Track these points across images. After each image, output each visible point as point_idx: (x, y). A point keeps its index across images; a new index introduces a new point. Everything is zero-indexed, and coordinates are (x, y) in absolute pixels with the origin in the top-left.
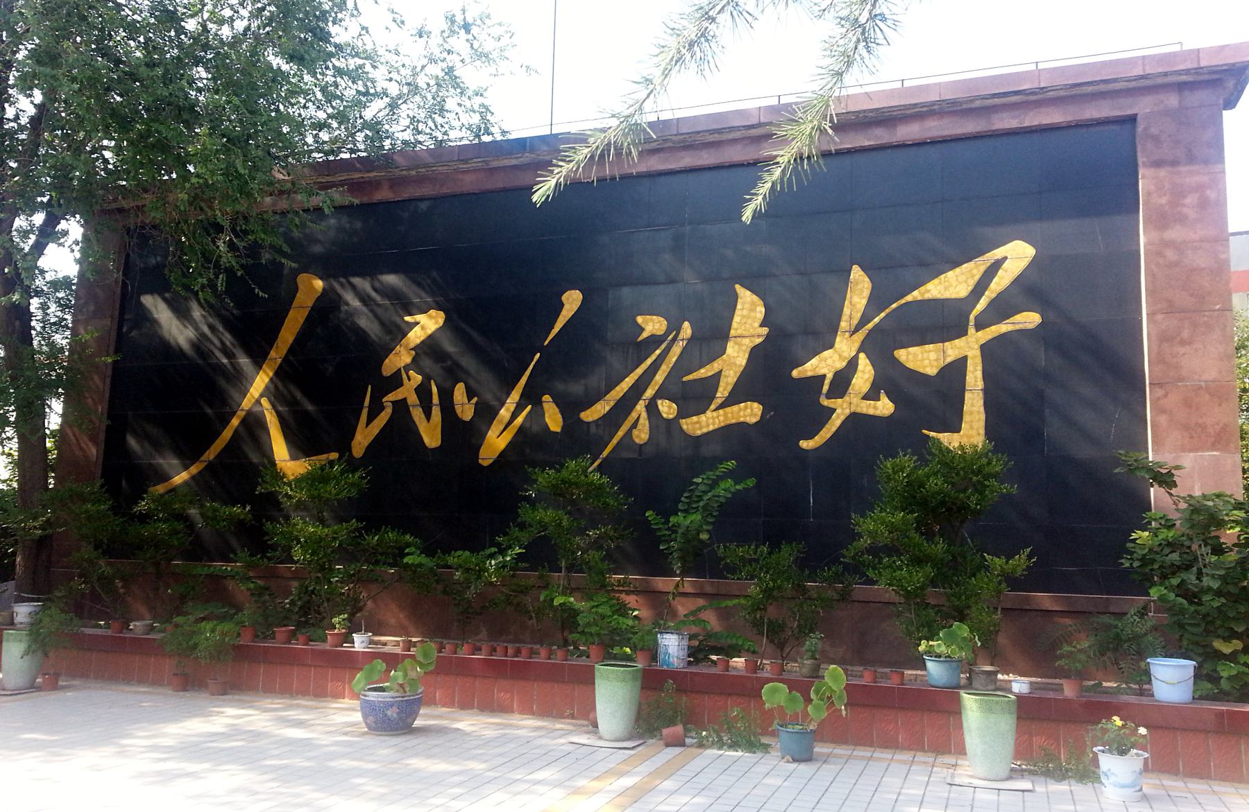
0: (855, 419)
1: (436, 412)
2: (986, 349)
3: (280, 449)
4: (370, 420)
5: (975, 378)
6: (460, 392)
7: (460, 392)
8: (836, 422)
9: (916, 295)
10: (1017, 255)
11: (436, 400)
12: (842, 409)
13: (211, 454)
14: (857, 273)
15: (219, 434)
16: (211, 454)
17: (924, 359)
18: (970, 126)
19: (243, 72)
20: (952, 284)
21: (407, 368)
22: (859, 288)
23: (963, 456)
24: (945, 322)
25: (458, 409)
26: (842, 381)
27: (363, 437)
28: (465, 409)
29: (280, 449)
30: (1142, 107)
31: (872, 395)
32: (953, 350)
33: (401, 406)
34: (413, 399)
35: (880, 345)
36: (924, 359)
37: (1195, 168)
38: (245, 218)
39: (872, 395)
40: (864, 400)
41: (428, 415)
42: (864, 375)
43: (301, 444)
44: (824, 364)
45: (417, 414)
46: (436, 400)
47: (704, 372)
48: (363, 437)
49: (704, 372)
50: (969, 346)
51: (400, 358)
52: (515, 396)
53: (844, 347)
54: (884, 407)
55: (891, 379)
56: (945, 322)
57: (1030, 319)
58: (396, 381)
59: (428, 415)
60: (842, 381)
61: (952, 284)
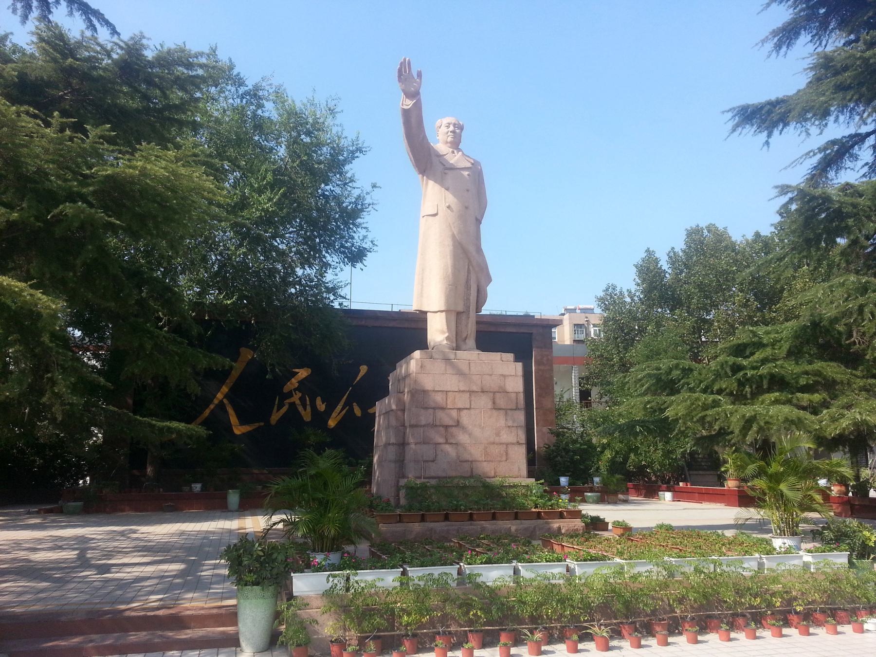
1: (309, 408)
3: (233, 419)
4: (278, 410)
6: (319, 401)
7: (319, 401)
11: (308, 403)
15: (201, 413)
18: (493, 329)
21: (295, 390)
23: (626, 492)
25: (318, 407)
27: (275, 417)
28: (321, 406)
29: (233, 419)
33: (293, 405)
34: (298, 402)
38: (786, 592)
41: (305, 409)
43: (243, 420)
45: (300, 409)
46: (308, 403)
47: (297, 370)
48: (275, 417)
49: (297, 370)
52: (203, 574)
58: (290, 394)
59: (305, 409)
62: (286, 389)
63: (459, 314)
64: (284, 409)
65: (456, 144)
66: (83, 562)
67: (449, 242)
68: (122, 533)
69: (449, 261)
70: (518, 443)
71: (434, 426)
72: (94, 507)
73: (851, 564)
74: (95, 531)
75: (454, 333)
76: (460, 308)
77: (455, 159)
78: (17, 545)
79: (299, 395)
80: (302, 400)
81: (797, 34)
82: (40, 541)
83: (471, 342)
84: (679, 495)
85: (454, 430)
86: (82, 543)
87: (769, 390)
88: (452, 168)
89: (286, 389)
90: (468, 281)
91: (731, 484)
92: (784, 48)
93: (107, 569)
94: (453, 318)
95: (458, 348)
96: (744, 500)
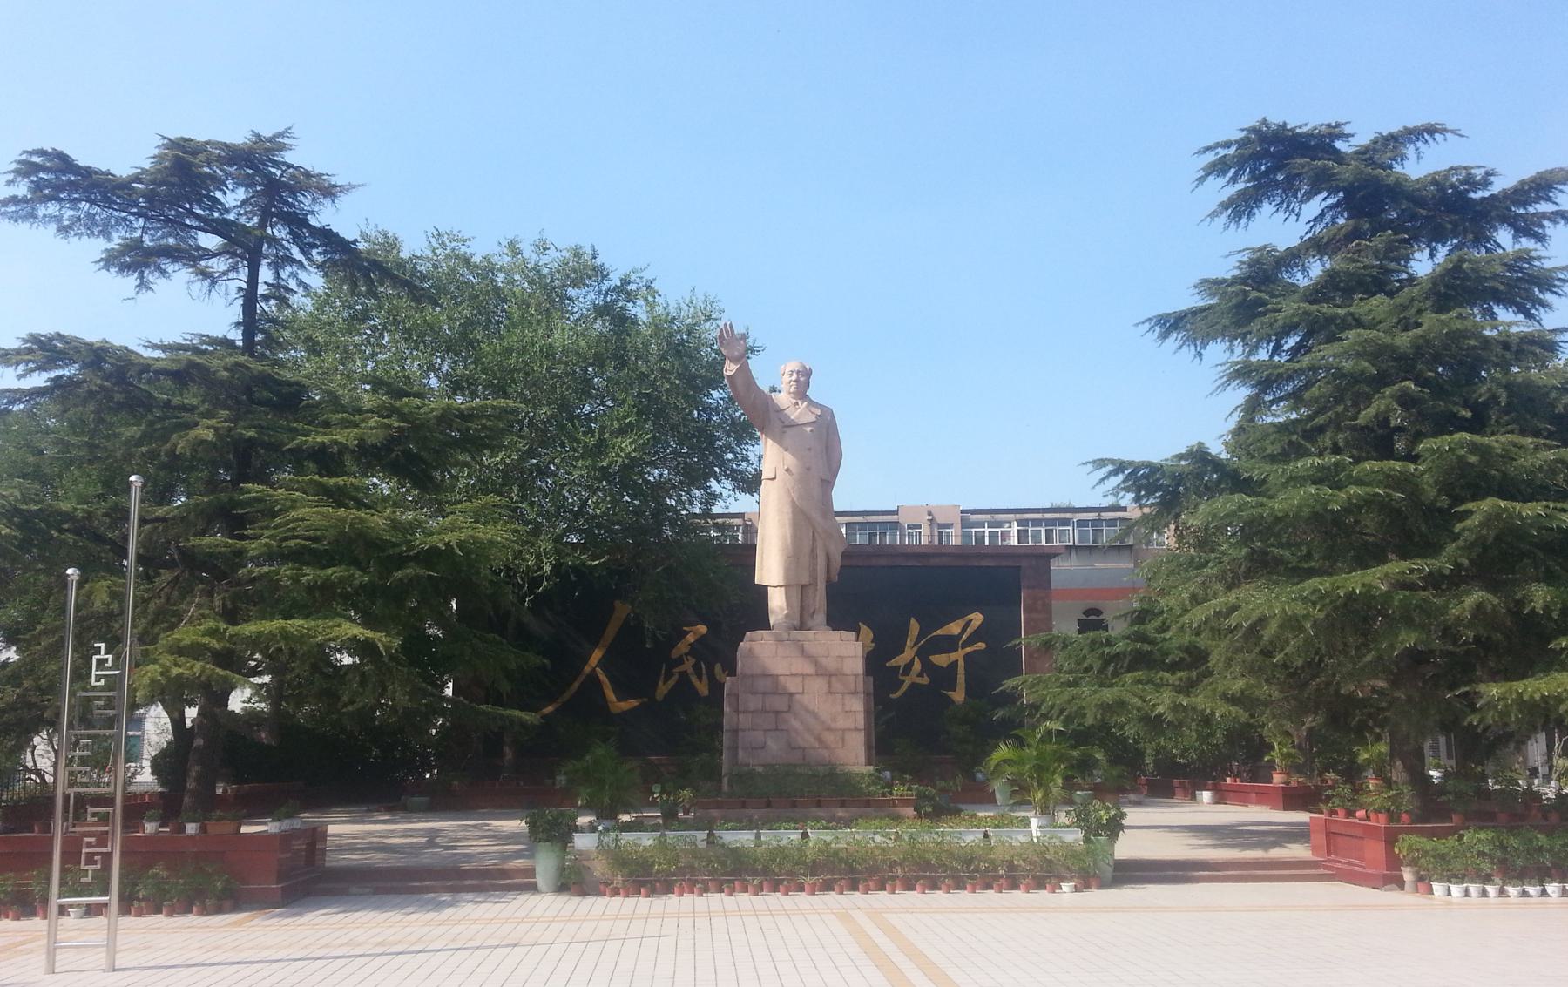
0: (913, 686)
1: (705, 677)
2: (967, 657)
3: (611, 695)
5: (961, 663)
8: (904, 688)
9: (939, 632)
10: (977, 618)
12: (907, 681)
13: (611, 632)
14: (913, 621)
16: (611, 632)
17: (941, 660)
18: (962, 563)
19: (543, 422)
20: (954, 628)
22: (915, 626)
24: (950, 644)
26: (910, 665)
27: (663, 689)
29: (611, 695)
30: (1024, 563)
31: (920, 675)
32: (954, 656)
33: (684, 674)
34: (690, 670)
35: (923, 654)
36: (941, 660)
37: (869, 809)
39: (920, 675)
40: (916, 677)
41: (700, 679)
42: (917, 666)
44: (900, 660)
45: (694, 679)
48: (663, 689)
50: (958, 656)
51: (682, 648)
53: (909, 653)
54: (925, 680)
55: (928, 667)
56: (950, 644)
57: (981, 645)
58: (680, 661)
60: (910, 665)
61: (954, 628)
62: (675, 654)
63: (803, 586)
64: (671, 683)
65: (801, 392)
66: (432, 843)
67: (788, 509)
68: (475, 826)
69: (788, 531)
70: (856, 729)
71: (764, 711)
72: (443, 801)
73: (1087, 840)
74: (446, 825)
75: (797, 610)
76: (805, 580)
77: (799, 413)
78: (371, 833)
79: (692, 661)
80: (696, 667)
81: (1258, 202)
82: (392, 831)
83: (821, 617)
84: (1221, 798)
85: (786, 716)
86: (432, 835)
87: (1130, 669)
88: (793, 425)
89: (675, 654)
90: (813, 550)
91: (1277, 779)
92: (1244, 220)
93: (455, 848)
94: (796, 593)
95: (802, 626)
96: (1292, 799)
